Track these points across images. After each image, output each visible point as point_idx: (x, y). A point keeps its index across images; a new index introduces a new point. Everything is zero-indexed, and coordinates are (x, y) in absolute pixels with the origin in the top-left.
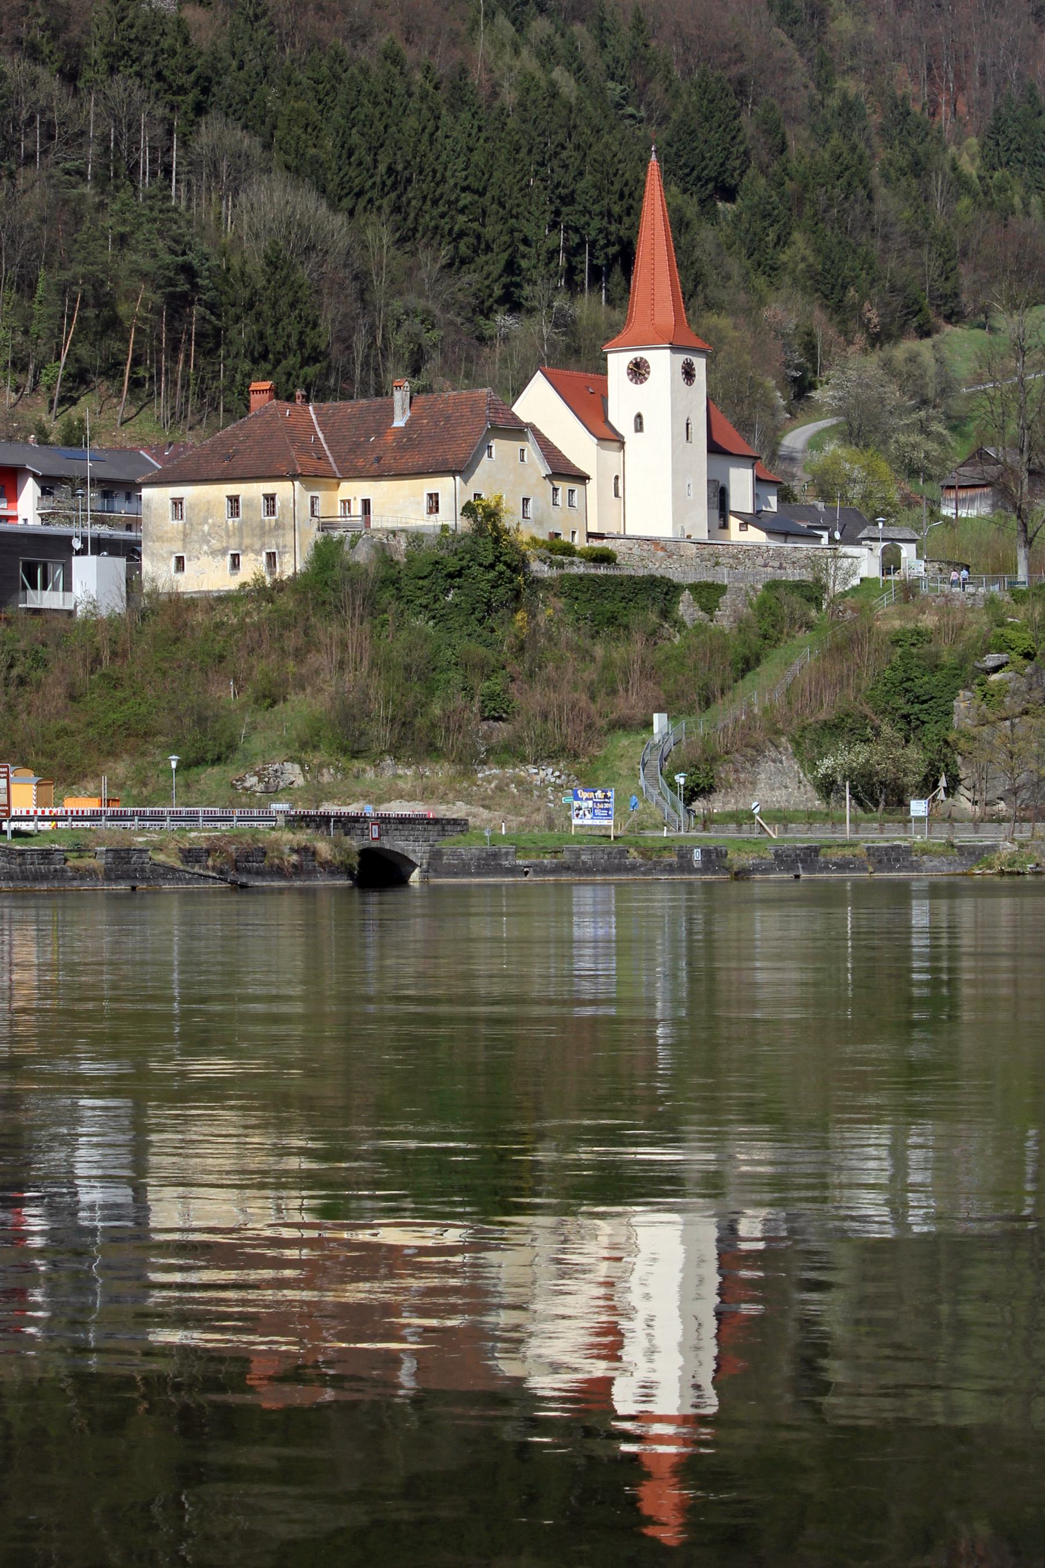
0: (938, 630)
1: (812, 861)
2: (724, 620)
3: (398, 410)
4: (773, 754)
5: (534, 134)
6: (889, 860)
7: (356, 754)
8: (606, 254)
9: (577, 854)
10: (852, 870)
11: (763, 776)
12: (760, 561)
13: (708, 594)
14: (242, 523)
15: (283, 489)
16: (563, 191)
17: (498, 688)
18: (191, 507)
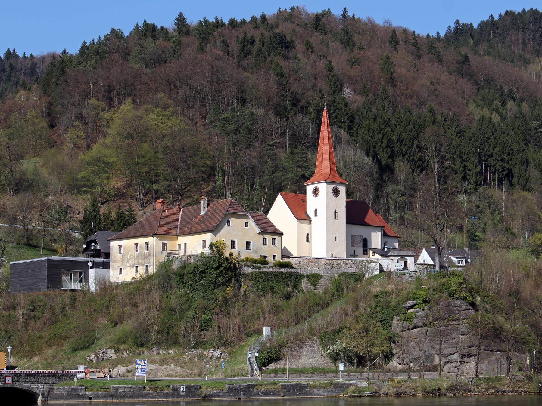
0: (393, 291)
1: (249, 391)
2: (320, 290)
3: (202, 208)
4: (310, 343)
5: (479, 134)
6: (294, 391)
7: (142, 345)
8: (503, 174)
9: (117, 389)
10: (273, 395)
11: (304, 353)
12: (349, 265)
13: (314, 279)
14: (139, 254)
15: (150, 240)
16: (489, 153)
17: (208, 318)
18: (124, 249)
